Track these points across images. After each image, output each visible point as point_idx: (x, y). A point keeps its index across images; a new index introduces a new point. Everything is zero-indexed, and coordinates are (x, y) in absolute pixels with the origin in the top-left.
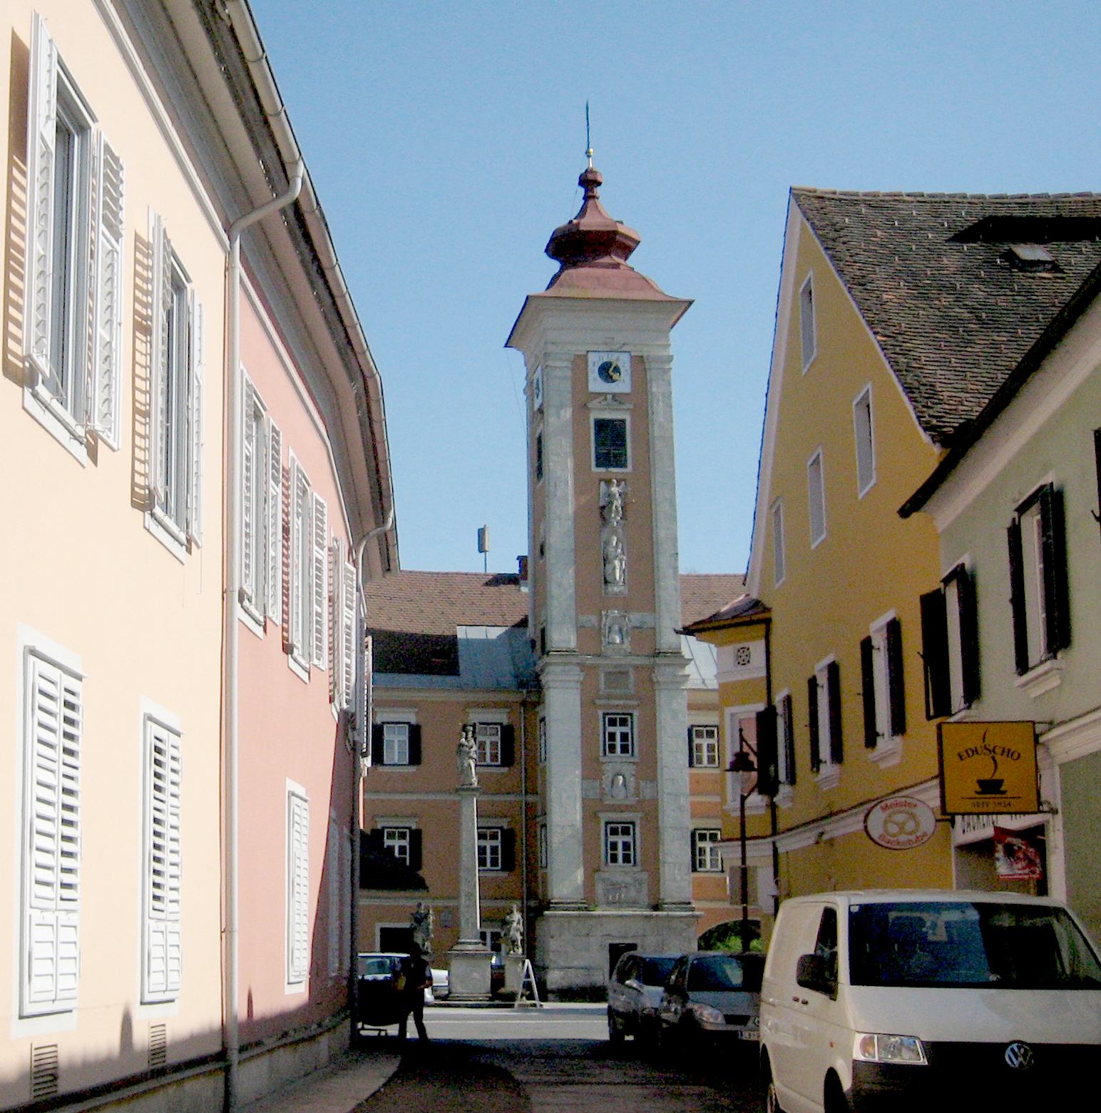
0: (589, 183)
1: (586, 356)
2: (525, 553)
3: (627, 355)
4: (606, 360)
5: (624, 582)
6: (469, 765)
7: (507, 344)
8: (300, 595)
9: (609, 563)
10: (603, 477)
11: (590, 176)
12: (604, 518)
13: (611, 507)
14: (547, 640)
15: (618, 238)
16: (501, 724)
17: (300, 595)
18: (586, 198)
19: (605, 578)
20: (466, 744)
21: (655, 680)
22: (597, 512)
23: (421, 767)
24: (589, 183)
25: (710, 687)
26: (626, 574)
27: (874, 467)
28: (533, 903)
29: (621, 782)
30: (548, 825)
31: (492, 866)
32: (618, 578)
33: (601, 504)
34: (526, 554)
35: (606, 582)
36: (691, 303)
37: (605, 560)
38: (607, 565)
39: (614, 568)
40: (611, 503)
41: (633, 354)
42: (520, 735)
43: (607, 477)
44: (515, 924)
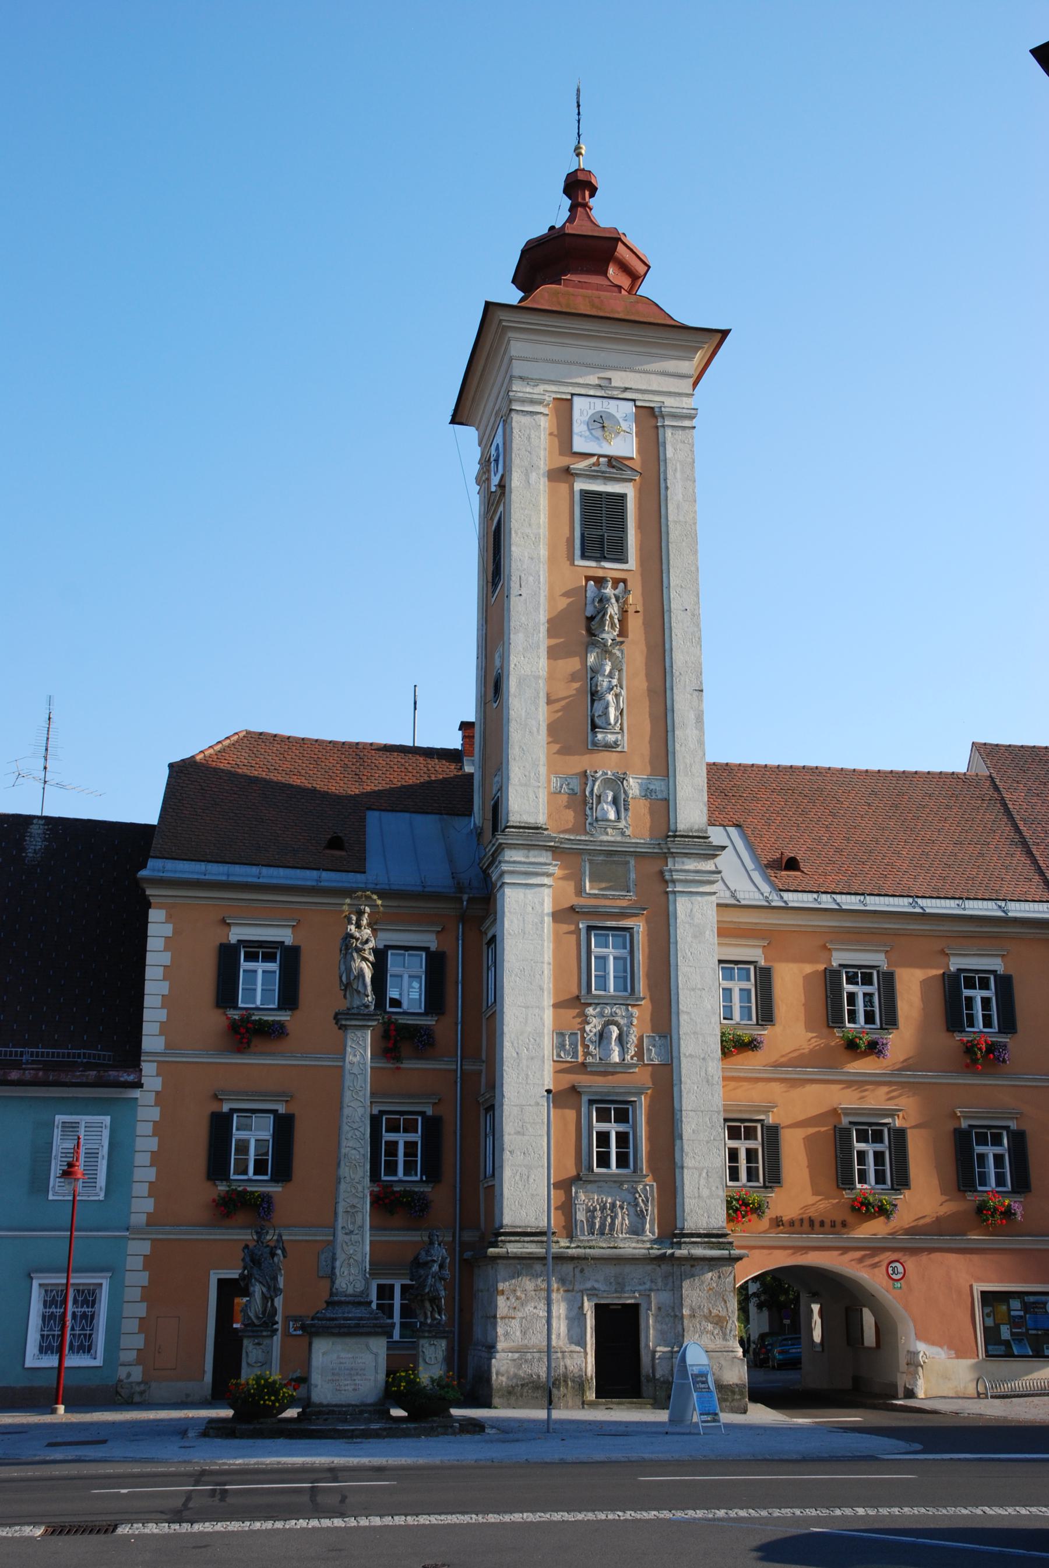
0: (579, 187)
1: (571, 400)
2: (471, 717)
3: (631, 404)
4: (599, 408)
5: (621, 729)
6: (361, 970)
7: (454, 416)
8: (456, 1348)
9: (600, 699)
10: (591, 573)
11: (581, 176)
12: (591, 633)
13: (604, 615)
14: (502, 815)
15: (620, 247)
16: (426, 949)
17: (456, 1348)
18: (573, 209)
19: (593, 721)
20: (357, 935)
21: (667, 877)
22: (583, 623)
23: (297, 1013)
24: (579, 187)
25: (743, 902)
26: (625, 717)
27: (541, 1414)
28: (469, 1236)
29: (615, 1035)
30: (496, 1107)
31: (405, 1174)
32: (612, 721)
33: (589, 615)
34: (472, 719)
35: (594, 726)
36: (725, 333)
37: (592, 695)
38: (596, 703)
39: (607, 707)
40: (602, 611)
41: (638, 403)
42: (456, 970)
43: (600, 573)
44: (435, 1268)
